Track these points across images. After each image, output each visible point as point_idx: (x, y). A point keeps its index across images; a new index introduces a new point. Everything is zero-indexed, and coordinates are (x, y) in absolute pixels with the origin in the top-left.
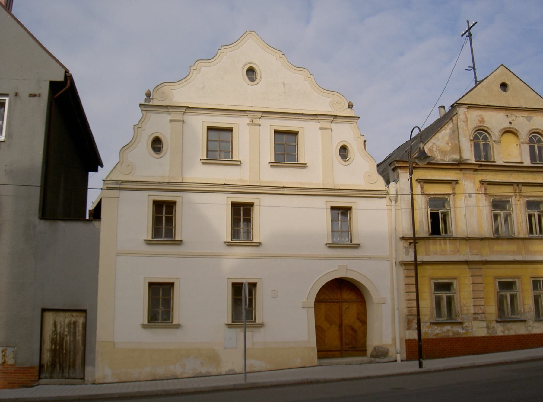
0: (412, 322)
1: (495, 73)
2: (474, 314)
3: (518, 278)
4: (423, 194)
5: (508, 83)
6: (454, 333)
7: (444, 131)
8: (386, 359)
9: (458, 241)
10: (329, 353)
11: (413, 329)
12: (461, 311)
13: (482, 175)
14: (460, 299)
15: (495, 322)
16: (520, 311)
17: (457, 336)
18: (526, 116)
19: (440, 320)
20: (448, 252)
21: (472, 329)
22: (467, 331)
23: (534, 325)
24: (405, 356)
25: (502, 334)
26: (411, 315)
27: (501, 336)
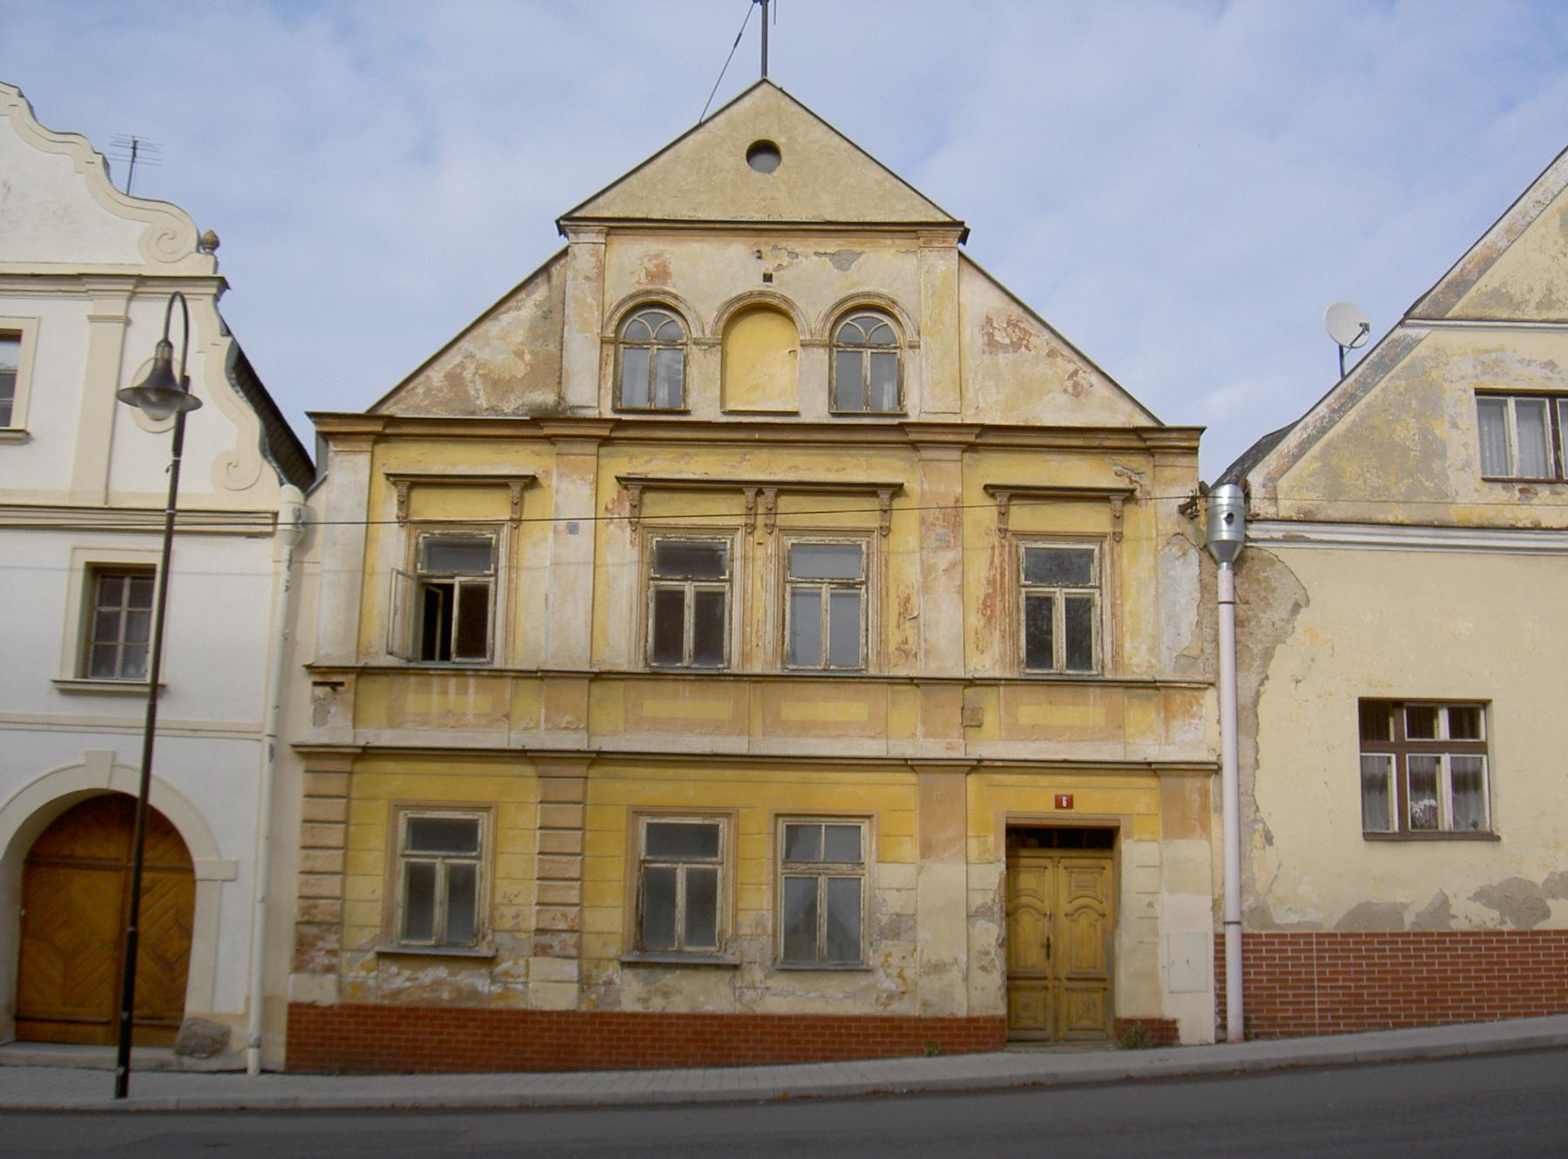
0: (312, 945)
1: (734, 108)
2: (540, 931)
3: (727, 815)
4: (404, 521)
5: (780, 141)
6: (459, 993)
7: (513, 314)
8: (214, 1063)
9: (509, 681)
10: (72, 1027)
11: (314, 971)
12: (492, 917)
13: (631, 457)
14: (494, 877)
15: (616, 964)
16: (722, 932)
17: (470, 1005)
18: (831, 250)
19: (417, 945)
20: (470, 717)
21: (526, 983)
22: (506, 989)
23: (770, 983)
24: (278, 1056)
25: (638, 1008)
26: (308, 923)
27: (633, 1015)
